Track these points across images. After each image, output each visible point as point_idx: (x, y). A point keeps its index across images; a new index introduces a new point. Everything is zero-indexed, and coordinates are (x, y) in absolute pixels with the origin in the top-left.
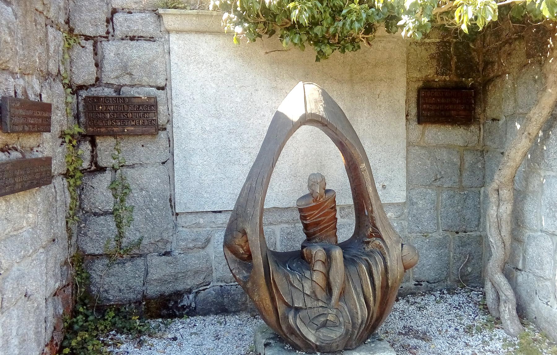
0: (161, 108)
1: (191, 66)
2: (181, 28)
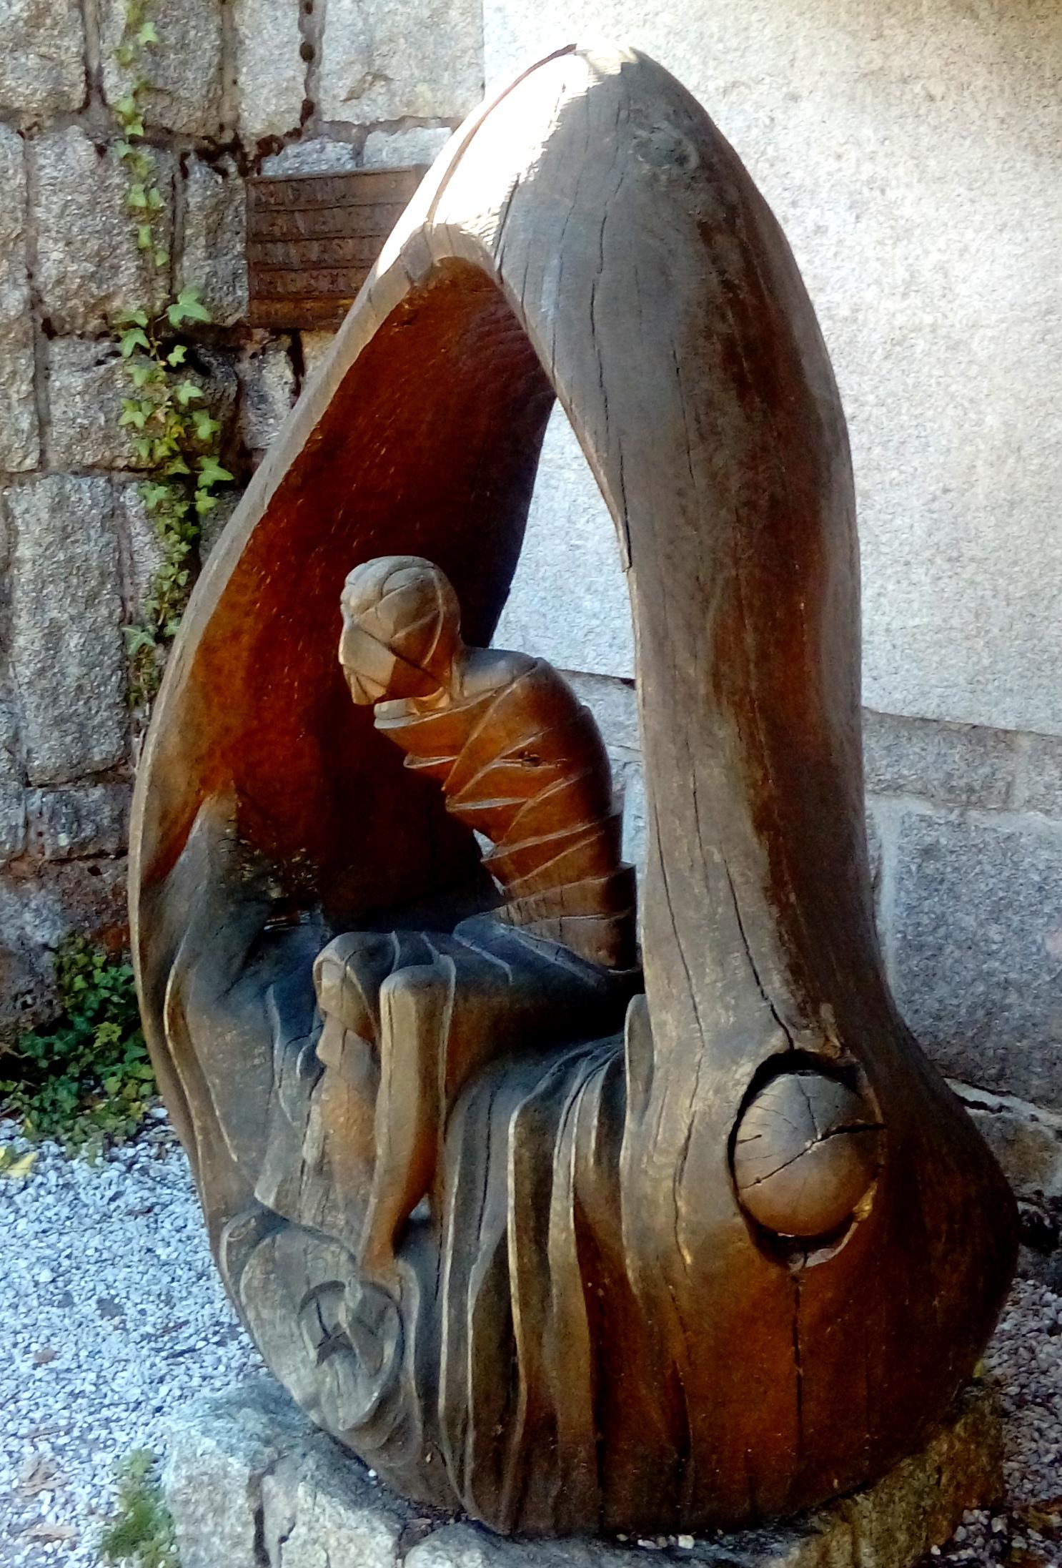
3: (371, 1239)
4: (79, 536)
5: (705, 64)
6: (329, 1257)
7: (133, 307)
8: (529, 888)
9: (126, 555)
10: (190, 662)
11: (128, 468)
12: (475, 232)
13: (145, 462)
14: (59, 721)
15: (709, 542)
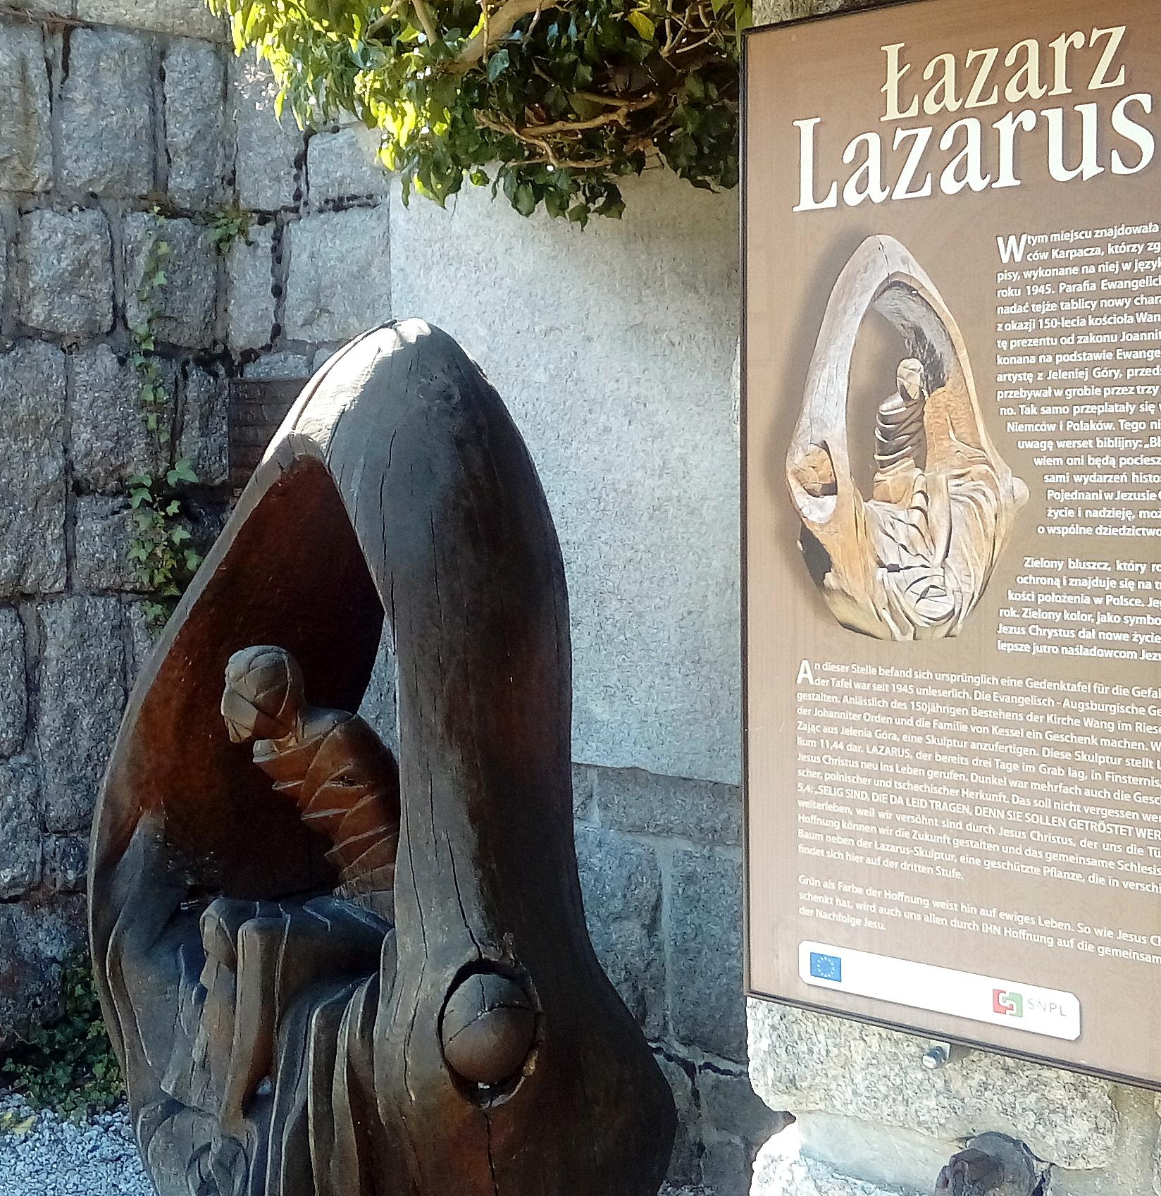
3: (228, 1104)
4: (93, 641)
5: (533, 314)
6: (207, 1127)
7: (142, 472)
9: (129, 657)
10: (134, 720)
11: (134, 591)
12: (317, 440)
13: (147, 587)
14: (72, 782)
15: (447, 638)
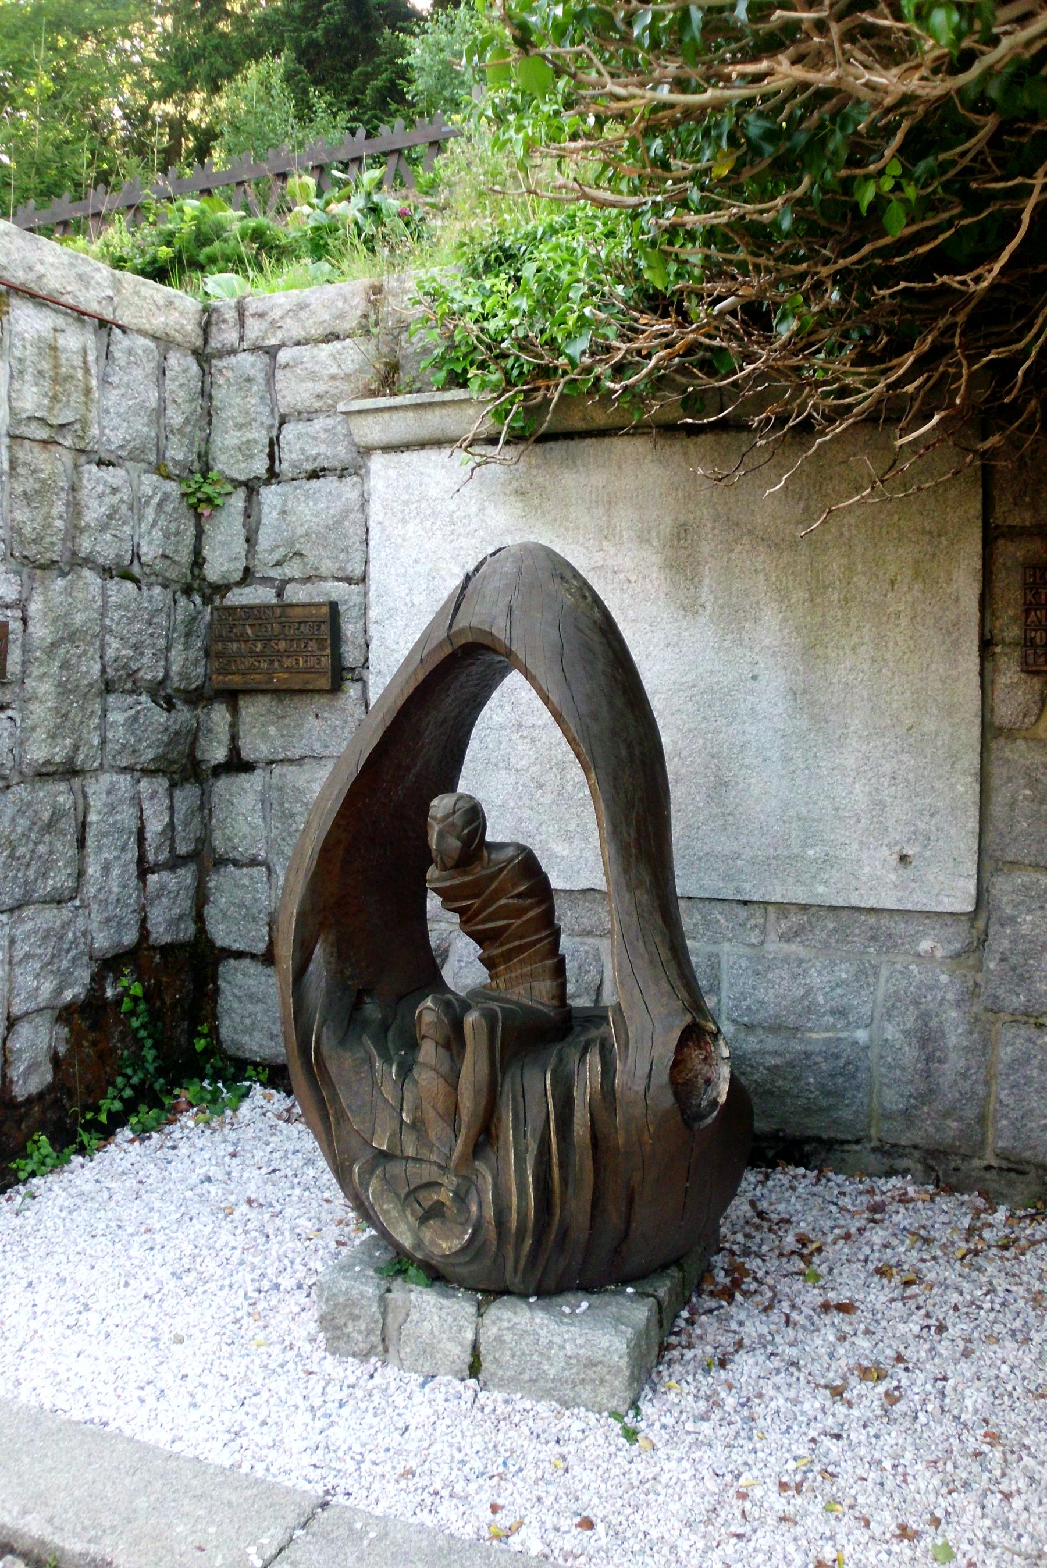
0: (350, 628)
1: (411, 527)
2: (424, 434)
8: (509, 970)
